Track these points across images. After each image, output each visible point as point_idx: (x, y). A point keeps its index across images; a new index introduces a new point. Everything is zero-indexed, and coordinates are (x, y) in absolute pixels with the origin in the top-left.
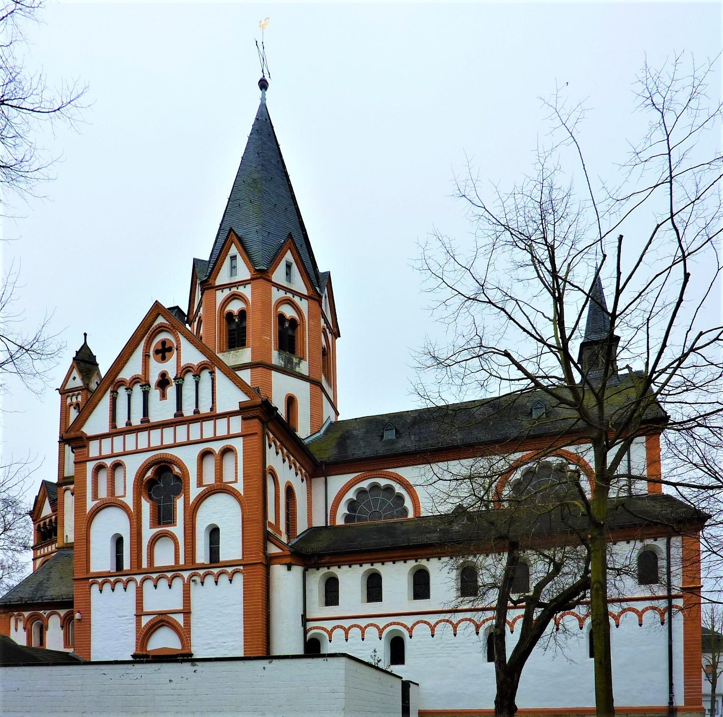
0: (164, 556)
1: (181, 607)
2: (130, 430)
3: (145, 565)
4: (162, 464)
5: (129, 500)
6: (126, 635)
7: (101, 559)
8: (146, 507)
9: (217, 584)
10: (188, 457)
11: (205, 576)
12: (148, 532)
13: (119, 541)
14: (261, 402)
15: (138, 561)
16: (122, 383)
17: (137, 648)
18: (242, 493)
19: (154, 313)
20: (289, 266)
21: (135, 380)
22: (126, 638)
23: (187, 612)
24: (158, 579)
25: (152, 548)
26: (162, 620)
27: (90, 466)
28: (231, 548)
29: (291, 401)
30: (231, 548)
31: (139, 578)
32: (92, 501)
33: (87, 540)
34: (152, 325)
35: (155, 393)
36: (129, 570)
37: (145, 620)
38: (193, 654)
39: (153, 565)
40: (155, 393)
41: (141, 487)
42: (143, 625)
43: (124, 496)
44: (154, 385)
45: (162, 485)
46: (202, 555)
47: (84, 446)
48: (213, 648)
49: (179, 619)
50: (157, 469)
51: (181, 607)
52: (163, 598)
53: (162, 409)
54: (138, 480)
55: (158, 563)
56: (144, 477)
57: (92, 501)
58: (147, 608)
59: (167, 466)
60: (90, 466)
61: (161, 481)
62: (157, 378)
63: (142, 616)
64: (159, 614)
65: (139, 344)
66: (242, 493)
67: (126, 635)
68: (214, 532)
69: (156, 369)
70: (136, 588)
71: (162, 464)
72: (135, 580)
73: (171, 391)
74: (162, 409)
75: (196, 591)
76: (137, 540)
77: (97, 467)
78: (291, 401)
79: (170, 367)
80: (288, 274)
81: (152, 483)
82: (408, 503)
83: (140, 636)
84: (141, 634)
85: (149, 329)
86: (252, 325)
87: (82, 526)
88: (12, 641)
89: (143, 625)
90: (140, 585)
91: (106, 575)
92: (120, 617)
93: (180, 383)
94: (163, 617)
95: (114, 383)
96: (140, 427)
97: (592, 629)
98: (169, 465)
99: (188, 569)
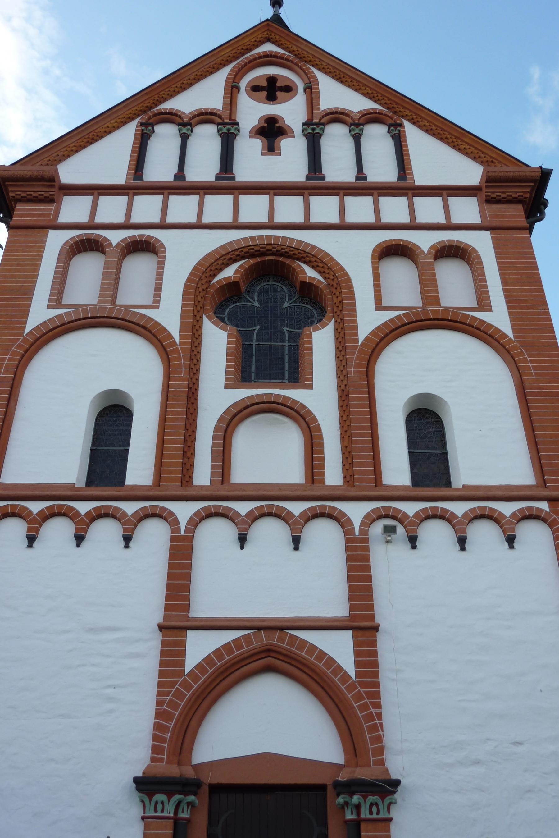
1: (339, 609)
3: (203, 475)
4: (267, 258)
5: (169, 316)
6: (110, 699)
8: (216, 341)
9: (463, 549)
11: (140, 520)
12: (216, 395)
13: (112, 418)
14: (540, 174)
15: (184, 464)
16: (171, 117)
17: (156, 750)
18: (509, 332)
19: (259, 35)
21: (205, 117)
22: (111, 711)
23: (362, 625)
24: (255, 517)
25: (230, 429)
26: (270, 650)
27: (56, 240)
31: (184, 511)
32: (49, 307)
33: (10, 394)
34: (251, 50)
36: (151, 486)
37: (199, 647)
38: (396, 783)
39: (191, 477)
41: (204, 298)
42: (192, 659)
43: (155, 305)
44: (299, 91)
45: (256, 304)
46: (397, 469)
47: (51, 200)
48: (477, 762)
49: (340, 648)
50: (251, 267)
51: (339, 609)
54: (201, 279)
55: (242, 473)
56: (215, 276)
57: (49, 307)
58: (202, 606)
59: (283, 263)
60: (56, 240)
62: (256, 123)
63: (190, 633)
64: (260, 628)
65: (218, 69)
66: (509, 332)
67: (110, 699)
70: (173, 539)
71: (267, 258)
72: (169, 518)
75: (389, 561)
76: (188, 408)
77: (76, 243)
81: (232, 289)
83: (174, 706)
84: (179, 695)
85: (243, 54)
87: (6, 353)
89: (192, 659)
90: (187, 529)
91: (57, 500)
92: (91, 630)
93: (316, 131)
94: (275, 640)
95: (150, 113)
96: (214, 184)
98: (288, 261)
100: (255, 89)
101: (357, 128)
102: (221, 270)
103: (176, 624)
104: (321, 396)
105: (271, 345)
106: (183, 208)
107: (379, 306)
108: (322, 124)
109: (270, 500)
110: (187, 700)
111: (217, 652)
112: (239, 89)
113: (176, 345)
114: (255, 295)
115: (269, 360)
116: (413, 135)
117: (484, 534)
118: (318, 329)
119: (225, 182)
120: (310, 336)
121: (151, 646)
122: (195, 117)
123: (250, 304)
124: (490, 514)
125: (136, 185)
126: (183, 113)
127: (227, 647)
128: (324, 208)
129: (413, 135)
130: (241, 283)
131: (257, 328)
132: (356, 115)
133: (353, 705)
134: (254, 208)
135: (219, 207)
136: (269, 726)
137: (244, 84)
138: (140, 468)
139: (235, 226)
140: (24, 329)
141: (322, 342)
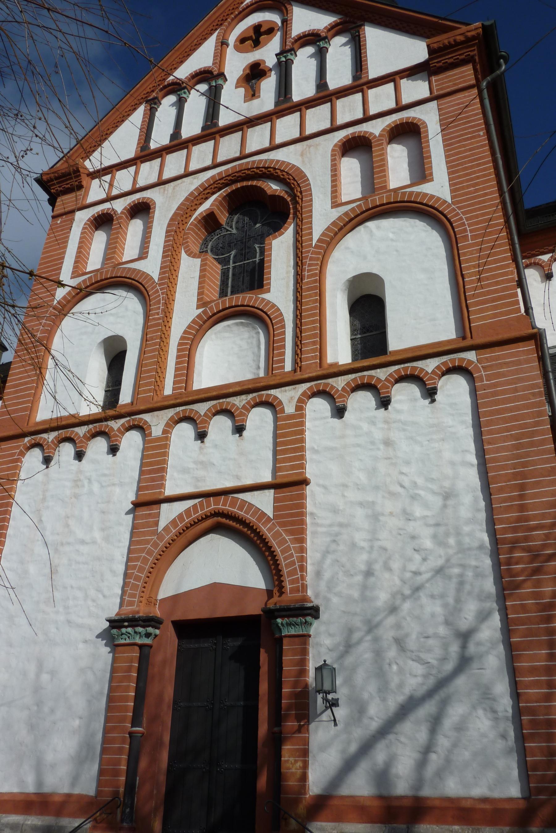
23: (290, 485)
26: (219, 515)
28: (421, 314)
30: (421, 314)
46: (339, 347)
52: (226, 459)
68: (368, 307)
81: (210, 222)
94: (222, 505)
100: (242, 40)
102: (201, 204)
103: (146, 504)
105: (244, 264)
107: (336, 204)
108: (293, 51)
109: (228, 402)
110: (151, 554)
111: (180, 516)
112: (228, 45)
113: (206, 310)
114: (234, 223)
117: (405, 395)
118: (276, 237)
119: (212, 131)
120: (271, 244)
122: (329, 30)
123: (229, 232)
124: (412, 373)
125: (146, 154)
126: (319, 30)
127: (188, 511)
128: (287, 127)
130: (218, 213)
131: (233, 253)
132: (323, 32)
134: (229, 147)
136: (219, 566)
137: (232, 39)
139: (215, 166)
140: (157, 524)
141: (280, 250)
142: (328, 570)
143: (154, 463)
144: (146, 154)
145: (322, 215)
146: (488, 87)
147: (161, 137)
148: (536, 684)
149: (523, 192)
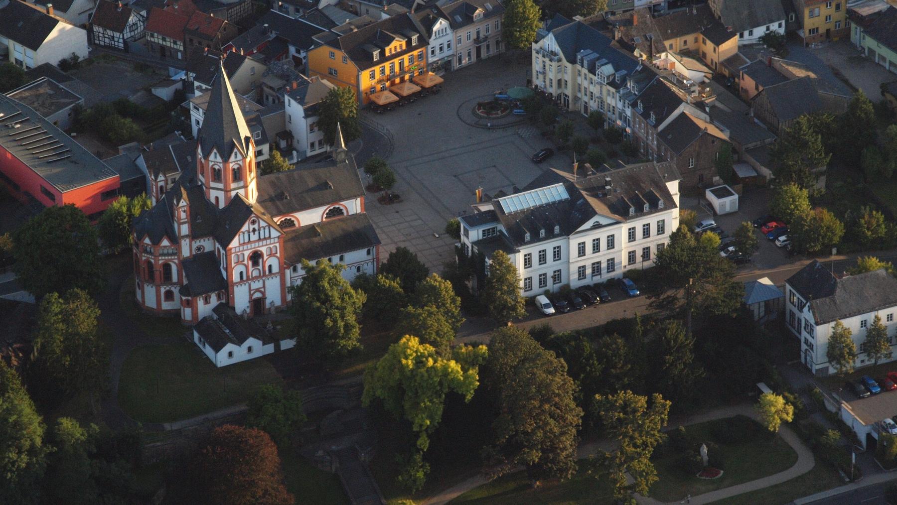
0: (256, 273)
2: (265, 239)
7: (236, 278)
10: (264, 250)
12: (251, 269)
13: (241, 273)
20: (236, 154)
23: (264, 287)
26: (258, 290)
28: (275, 269)
29: (217, 198)
30: (275, 269)
35: (252, 234)
40: (252, 234)
46: (267, 273)
52: (256, 285)
53: (254, 237)
61: (256, 257)
68: (270, 267)
69: (252, 227)
73: (257, 233)
74: (254, 237)
75: (267, 282)
78: (217, 198)
79: (256, 226)
80: (216, 157)
82: (296, 223)
86: (230, 176)
88: (516, 213)
97: (54, 200)
99: (262, 276)
101: (258, 164)
103: (250, 290)
104: (260, 267)
106: (245, 247)
109: (256, 278)
110: (251, 296)
115: (255, 264)
116: (272, 229)
121: (878, 397)
128: (261, 243)
129: (272, 229)
133: (263, 293)
134: (253, 246)
135: (249, 246)
136: (258, 295)
138: (245, 278)
141: (261, 261)
142: (268, 294)
143: (250, 285)
144: (240, 245)
145: (265, 257)
146: (355, 158)
147: (242, 242)
148: (392, 68)
149: (214, 361)
